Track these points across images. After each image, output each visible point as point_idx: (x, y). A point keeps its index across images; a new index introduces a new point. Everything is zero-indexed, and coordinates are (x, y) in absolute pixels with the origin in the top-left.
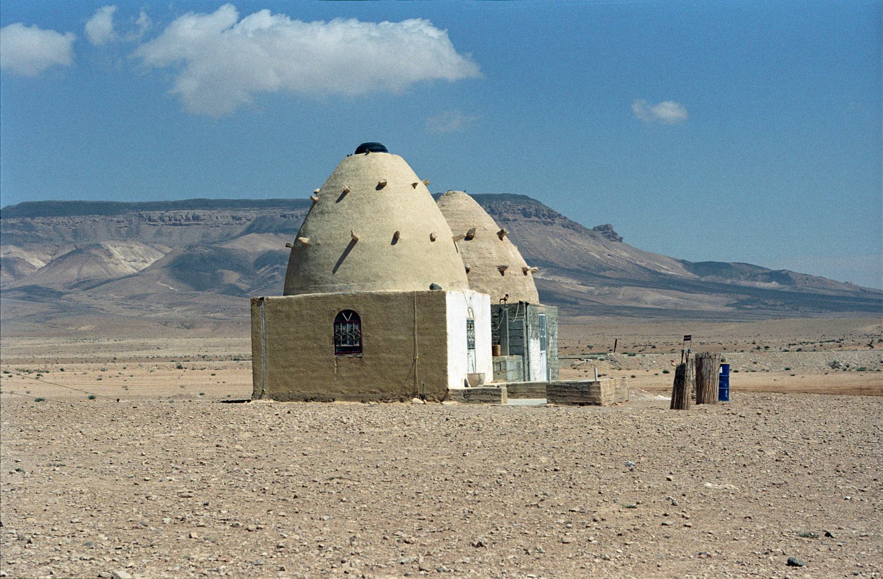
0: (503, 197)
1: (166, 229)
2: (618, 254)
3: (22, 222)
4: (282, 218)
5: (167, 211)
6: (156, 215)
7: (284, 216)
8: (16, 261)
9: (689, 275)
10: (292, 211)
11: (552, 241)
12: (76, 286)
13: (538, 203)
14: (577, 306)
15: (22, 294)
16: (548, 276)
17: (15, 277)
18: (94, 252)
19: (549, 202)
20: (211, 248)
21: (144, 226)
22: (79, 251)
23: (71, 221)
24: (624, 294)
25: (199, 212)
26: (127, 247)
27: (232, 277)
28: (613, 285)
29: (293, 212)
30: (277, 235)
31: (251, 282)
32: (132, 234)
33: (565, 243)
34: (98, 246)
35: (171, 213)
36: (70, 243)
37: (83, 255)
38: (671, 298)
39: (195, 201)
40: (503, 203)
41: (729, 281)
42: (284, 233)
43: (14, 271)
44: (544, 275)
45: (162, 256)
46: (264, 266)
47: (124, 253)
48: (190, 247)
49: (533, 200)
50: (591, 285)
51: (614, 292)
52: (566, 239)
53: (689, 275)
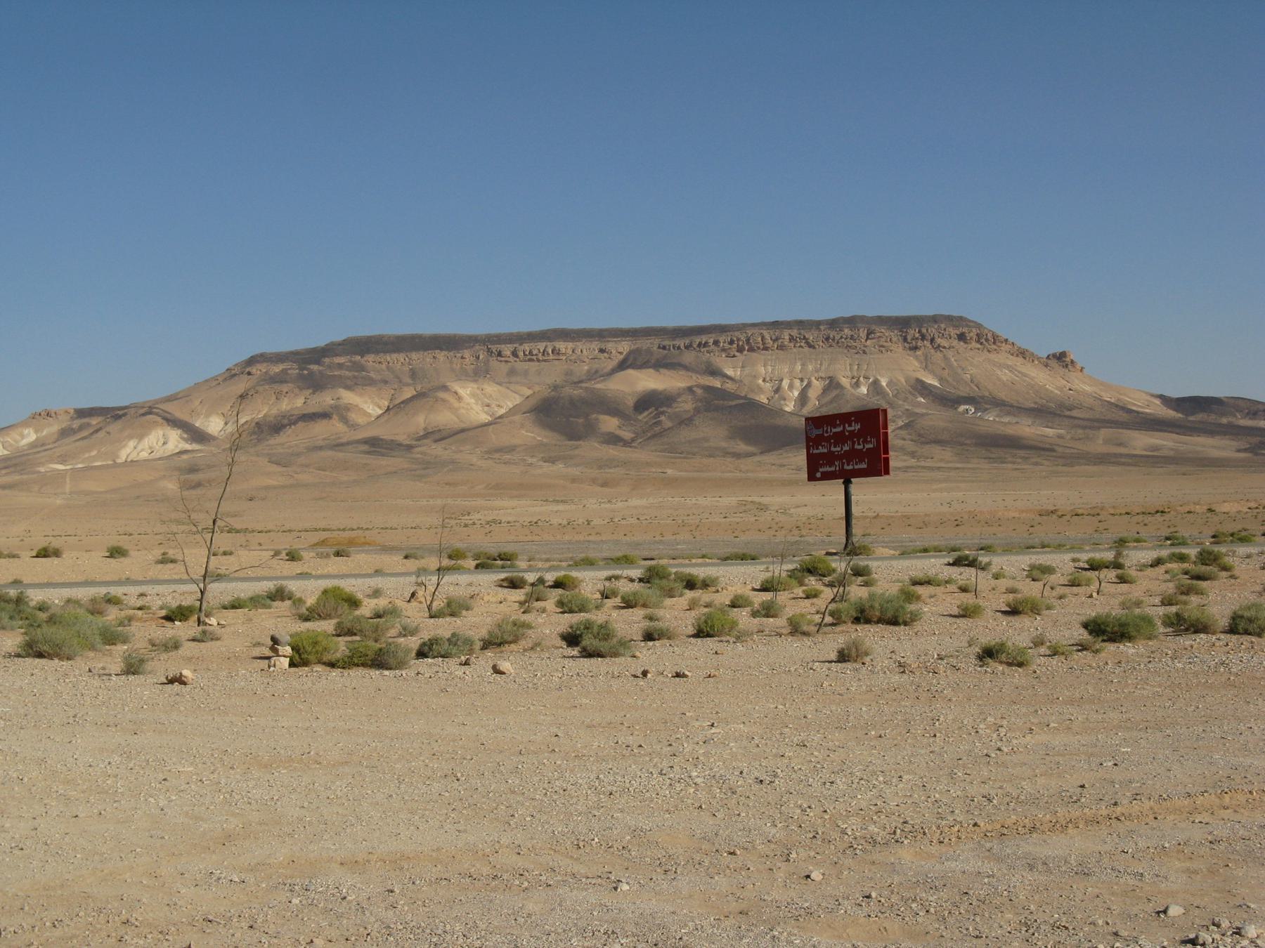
0: (935, 319)
1: (521, 366)
2: (1080, 386)
3: (351, 361)
4: (661, 350)
5: (521, 344)
6: (507, 350)
7: (664, 348)
8: (348, 408)
9: (1171, 414)
10: (673, 340)
11: (999, 373)
12: (425, 436)
13: (979, 326)
14: (1054, 454)
15: (366, 447)
16: (1001, 417)
17: (348, 427)
18: (441, 395)
19: (991, 324)
20: (581, 388)
21: (494, 362)
22: (420, 396)
23: (407, 359)
24: (1100, 442)
25: (561, 345)
26: (478, 388)
27: (610, 424)
28: (1091, 428)
29: (674, 343)
30: (658, 371)
31: (633, 428)
32: (480, 373)
33: (1015, 375)
34: (445, 388)
35: (527, 347)
36: (408, 385)
37: (428, 399)
38: (1165, 443)
39: (555, 331)
40: (936, 327)
41: (1224, 421)
42: (667, 368)
43: (347, 421)
44: (997, 416)
45: (518, 400)
46: (647, 409)
47: (473, 395)
48: (555, 387)
49: (973, 321)
50: (1059, 427)
51: (1091, 436)
52: (1016, 370)
53: (1171, 414)
